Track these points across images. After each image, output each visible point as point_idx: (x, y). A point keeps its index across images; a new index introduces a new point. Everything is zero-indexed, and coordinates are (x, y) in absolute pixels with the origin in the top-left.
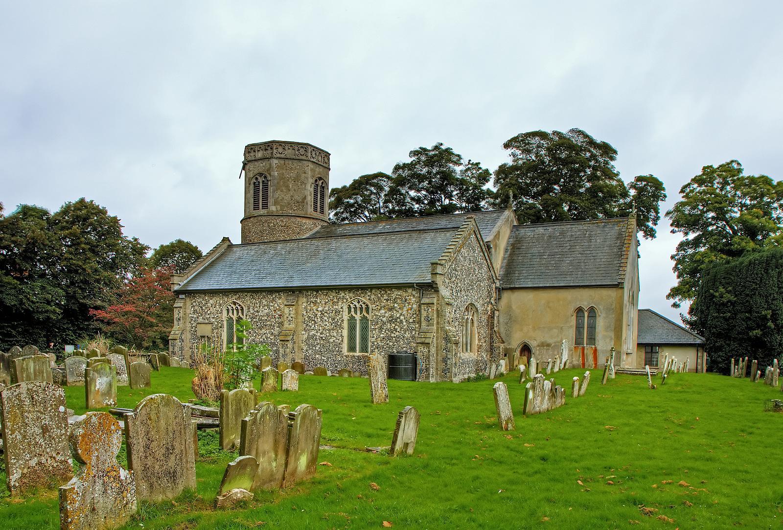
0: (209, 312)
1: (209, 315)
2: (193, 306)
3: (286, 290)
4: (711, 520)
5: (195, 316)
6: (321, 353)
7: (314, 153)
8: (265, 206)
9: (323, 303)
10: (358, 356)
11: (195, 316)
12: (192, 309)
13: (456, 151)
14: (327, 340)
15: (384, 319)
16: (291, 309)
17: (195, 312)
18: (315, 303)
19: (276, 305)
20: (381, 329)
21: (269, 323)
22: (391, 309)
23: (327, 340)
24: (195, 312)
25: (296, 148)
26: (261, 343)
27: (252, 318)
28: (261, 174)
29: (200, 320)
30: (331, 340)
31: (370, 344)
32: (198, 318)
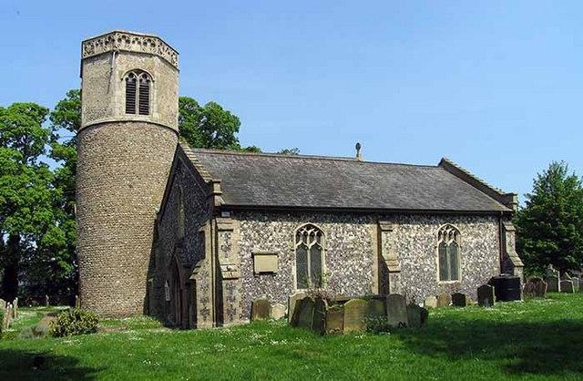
0: (271, 238)
1: (270, 242)
2: (244, 229)
3: (283, 211)
4: (104, 350)
5: (247, 244)
6: (416, 284)
7: (161, 48)
8: (145, 111)
9: (415, 230)
10: (452, 284)
11: (247, 244)
12: (242, 234)
13: (63, 97)
14: (420, 269)
15: (472, 246)
16: (388, 235)
17: (247, 237)
18: (407, 229)
19: (363, 231)
20: (470, 255)
21: (356, 252)
22: (476, 236)
23: (420, 269)
24: (247, 237)
25: (142, 41)
26: (348, 277)
27: (334, 247)
28: (139, 71)
29: (256, 249)
30: (426, 269)
31: (460, 271)
32: (252, 246)
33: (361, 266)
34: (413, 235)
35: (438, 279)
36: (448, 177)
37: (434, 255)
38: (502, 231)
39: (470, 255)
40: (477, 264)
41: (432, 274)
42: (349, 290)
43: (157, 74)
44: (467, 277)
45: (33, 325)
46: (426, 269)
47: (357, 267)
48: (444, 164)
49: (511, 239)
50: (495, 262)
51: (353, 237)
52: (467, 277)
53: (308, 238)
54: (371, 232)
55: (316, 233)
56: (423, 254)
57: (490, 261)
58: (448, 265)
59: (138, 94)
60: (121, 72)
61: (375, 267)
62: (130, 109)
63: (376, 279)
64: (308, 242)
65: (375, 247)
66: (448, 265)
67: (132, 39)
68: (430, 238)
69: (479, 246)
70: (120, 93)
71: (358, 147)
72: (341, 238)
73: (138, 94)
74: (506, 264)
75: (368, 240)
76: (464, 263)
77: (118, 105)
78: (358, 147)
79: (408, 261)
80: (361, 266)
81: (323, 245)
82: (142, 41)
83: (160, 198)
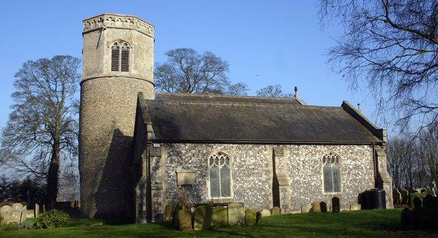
0: (190, 161)
1: (190, 164)
14: (309, 183)
15: (351, 167)
18: (297, 155)
19: (262, 156)
20: (349, 173)
23: (309, 183)
26: (250, 189)
28: (121, 41)
30: (313, 184)
33: (260, 181)
34: (302, 159)
35: (323, 191)
36: (349, 117)
37: (319, 173)
38: (375, 156)
39: (349, 173)
40: (356, 180)
41: (318, 187)
42: (251, 198)
43: (135, 43)
44: (347, 190)
45: (114, 73)
46: (313, 184)
47: (257, 182)
48: (345, 106)
49: (383, 161)
50: (370, 179)
51: (254, 161)
52: (347, 190)
53: (219, 161)
54: (268, 157)
55: (335, 157)
56: (310, 173)
57: (367, 178)
58: (332, 180)
59: (120, 57)
60: (108, 43)
61: (271, 182)
62: (115, 68)
63: (271, 191)
64: (219, 164)
65: (271, 168)
66: (332, 180)
67: (117, 18)
68: (316, 162)
69: (356, 167)
70: (107, 58)
71: (296, 89)
72: (245, 161)
73: (120, 57)
74: (379, 181)
75: (266, 162)
76: (345, 180)
77: (105, 65)
78: (296, 89)
79: (298, 178)
80: (260, 181)
81: (230, 167)
82: (124, 20)
83: (133, 131)
